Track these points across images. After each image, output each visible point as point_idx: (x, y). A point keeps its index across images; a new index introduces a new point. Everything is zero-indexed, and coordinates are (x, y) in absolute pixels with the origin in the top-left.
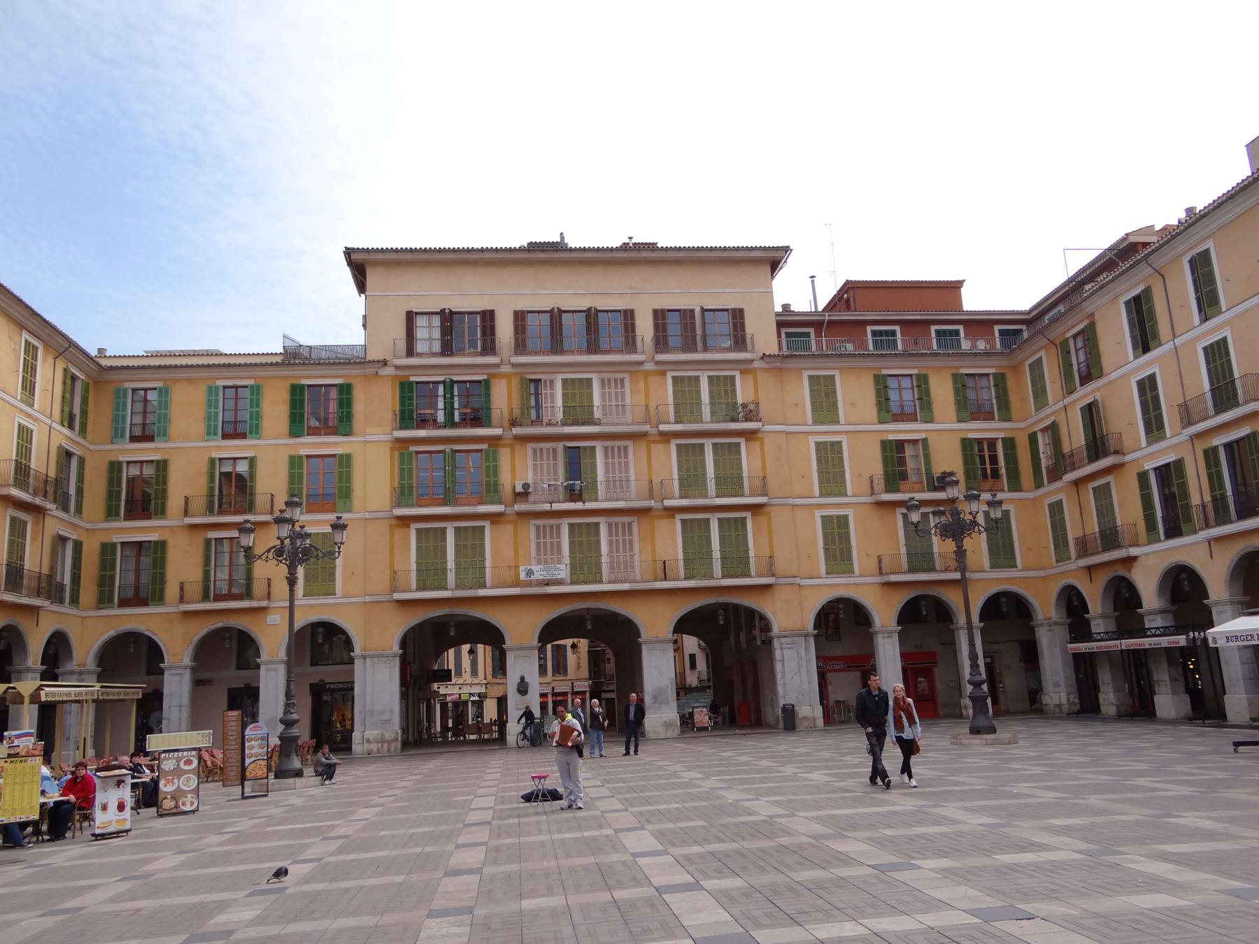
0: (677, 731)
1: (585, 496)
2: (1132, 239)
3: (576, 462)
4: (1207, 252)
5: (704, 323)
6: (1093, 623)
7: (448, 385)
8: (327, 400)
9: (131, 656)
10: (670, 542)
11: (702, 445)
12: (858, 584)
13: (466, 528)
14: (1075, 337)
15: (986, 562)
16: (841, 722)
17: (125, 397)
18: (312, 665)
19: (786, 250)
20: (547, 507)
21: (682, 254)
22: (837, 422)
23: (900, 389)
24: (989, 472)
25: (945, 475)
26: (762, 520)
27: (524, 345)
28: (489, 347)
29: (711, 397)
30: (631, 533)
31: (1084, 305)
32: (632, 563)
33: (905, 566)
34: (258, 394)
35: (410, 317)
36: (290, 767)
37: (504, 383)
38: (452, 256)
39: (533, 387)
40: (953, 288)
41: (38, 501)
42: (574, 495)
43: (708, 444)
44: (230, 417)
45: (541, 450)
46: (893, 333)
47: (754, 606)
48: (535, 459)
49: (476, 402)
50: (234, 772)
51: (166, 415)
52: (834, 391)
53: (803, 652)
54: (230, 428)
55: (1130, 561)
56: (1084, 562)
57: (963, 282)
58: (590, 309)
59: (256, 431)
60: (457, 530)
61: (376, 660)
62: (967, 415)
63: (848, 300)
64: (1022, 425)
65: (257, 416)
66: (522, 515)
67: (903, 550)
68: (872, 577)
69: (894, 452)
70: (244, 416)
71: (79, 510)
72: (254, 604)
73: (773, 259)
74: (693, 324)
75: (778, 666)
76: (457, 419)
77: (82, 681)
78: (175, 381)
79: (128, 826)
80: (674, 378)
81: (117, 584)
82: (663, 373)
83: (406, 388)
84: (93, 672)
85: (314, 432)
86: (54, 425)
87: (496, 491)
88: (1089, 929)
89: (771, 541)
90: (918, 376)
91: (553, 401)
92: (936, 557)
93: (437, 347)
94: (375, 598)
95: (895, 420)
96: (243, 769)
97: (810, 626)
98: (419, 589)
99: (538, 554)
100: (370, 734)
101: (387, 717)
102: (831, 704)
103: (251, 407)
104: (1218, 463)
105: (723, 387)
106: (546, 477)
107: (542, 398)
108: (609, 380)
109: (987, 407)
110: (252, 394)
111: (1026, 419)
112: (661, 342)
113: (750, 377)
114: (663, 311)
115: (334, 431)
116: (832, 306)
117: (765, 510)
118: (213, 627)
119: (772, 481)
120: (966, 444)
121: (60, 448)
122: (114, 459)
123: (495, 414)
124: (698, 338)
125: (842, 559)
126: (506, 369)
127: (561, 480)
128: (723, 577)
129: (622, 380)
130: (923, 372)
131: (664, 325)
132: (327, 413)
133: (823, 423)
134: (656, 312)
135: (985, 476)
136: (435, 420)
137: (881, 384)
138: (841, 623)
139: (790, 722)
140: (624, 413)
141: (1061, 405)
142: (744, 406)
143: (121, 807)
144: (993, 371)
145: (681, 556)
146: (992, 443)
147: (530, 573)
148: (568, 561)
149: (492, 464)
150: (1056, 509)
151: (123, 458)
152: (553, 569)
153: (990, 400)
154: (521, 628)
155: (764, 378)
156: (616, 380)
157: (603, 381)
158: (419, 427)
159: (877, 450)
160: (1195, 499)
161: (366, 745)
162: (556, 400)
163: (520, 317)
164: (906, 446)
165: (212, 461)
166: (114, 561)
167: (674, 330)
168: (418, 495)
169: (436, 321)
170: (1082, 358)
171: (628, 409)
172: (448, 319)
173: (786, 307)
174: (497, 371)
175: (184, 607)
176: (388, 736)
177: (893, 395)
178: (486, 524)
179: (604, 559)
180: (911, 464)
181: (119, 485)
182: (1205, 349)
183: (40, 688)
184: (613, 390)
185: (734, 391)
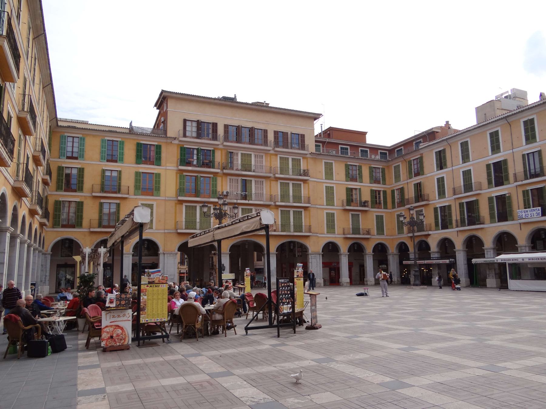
2: (434, 130)
3: (245, 185)
4: (467, 141)
6: (410, 255)
8: (150, 151)
11: (289, 183)
12: (337, 238)
14: (414, 160)
22: (333, 180)
28: (215, 137)
29: (292, 166)
33: (351, 232)
34: (123, 145)
35: (185, 121)
40: (363, 134)
42: (245, 197)
44: (110, 153)
46: (347, 149)
48: (230, 182)
52: (332, 168)
54: (110, 158)
59: (122, 160)
62: (349, 179)
67: (351, 227)
69: (350, 191)
73: (316, 117)
80: (280, 157)
82: (276, 155)
88: (358, 364)
89: (310, 219)
90: (382, 168)
91: (237, 161)
93: (195, 135)
101: (172, 277)
104: (463, 207)
105: (297, 162)
109: (355, 177)
111: (392, 185)
113: (305, 160)
122: (60, 165)
123: (216, 164)
126: (221, 147)
129: (262, 156)
131: (278, 137)
137: (347, 167)
141: (406, 182)
142: (304, 171)
146: (379, 191)
151: (64, 165)
155: (310, 161)
157: (255, 156)
160: (454, 218)
162: (238, 161)
163: (226, 127)
169: (195, 124)
170: (416, 167)
172: (199, 124)
182: (463, 172)
185: (300, 165)
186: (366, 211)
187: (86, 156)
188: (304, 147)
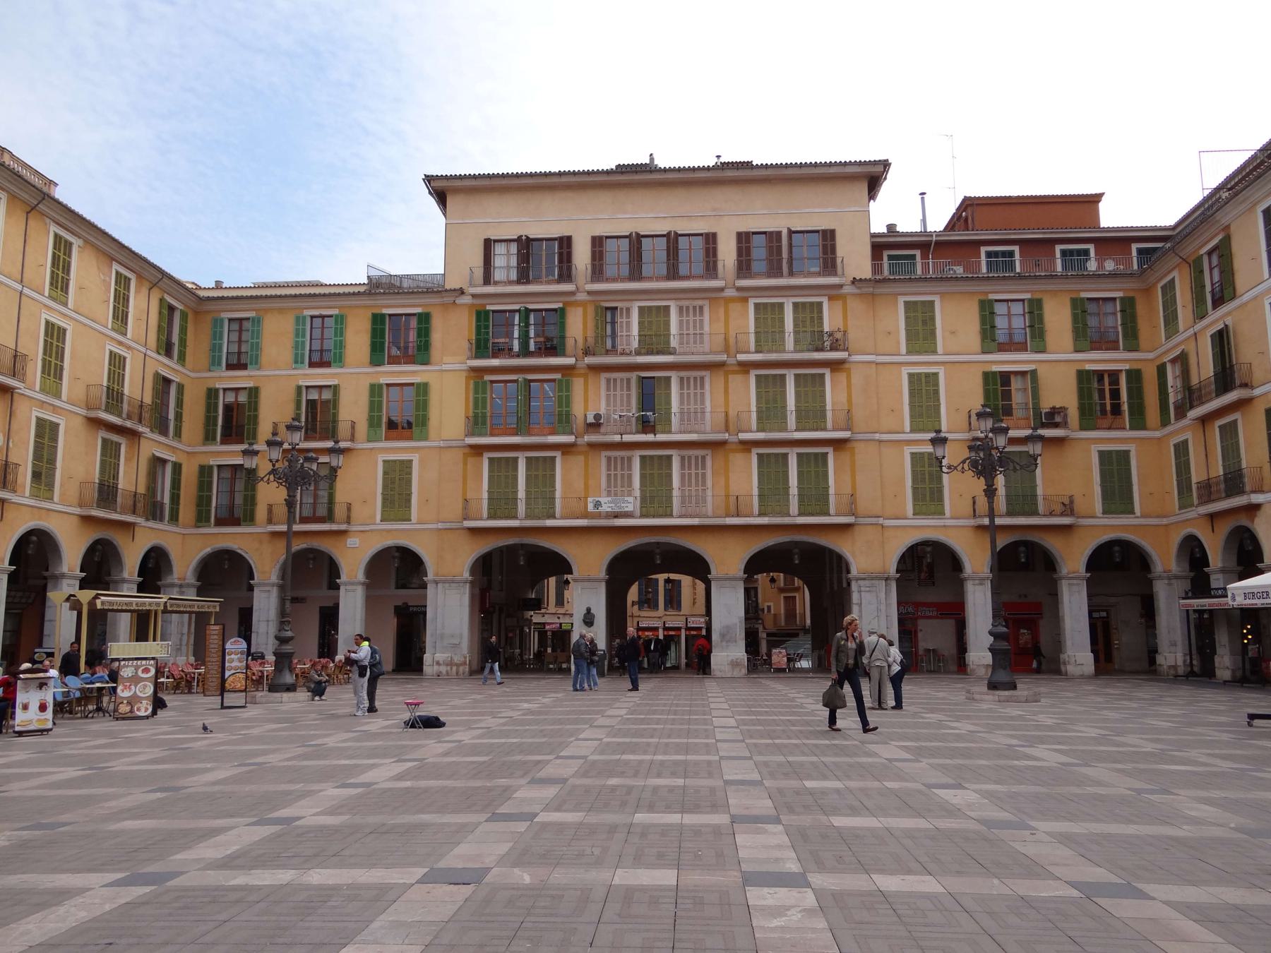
0: (744, 671)
1: (658, 427)
5: (790, 246)
6: (1212, 577)
7: (523, 314)
8: (408, 329)
9: (224, 572)
10: (745, 477)
11: (783, 376)
13: (537, 458)
14: (1210, 253)
16: (930, 672)
17: (222, 327)
18: (397, 588)
19: (886, 165)
20: (617, 438)
21: (769, 172)
22: (934, 352)
23: (1009, 315)
25: (1054, 412)
26: (845, 456)
27: (601, 271)
28: (566, 274)
29: (796, 325)
30: (704, 467)
31: (1218, 215)
35: (488, 244)
36: (282, 681)
37: (580, 311)
38: (473, 183)
39: (608, 315)
41: (128, 424)
43: (790, 376)
45: (615, 380)
46: (1011, 254)
47: (831, 547)
48: (608, 389)
49: (552, 331)
50: (214, 682)
51: (258, 344)
52: (933, 319)
53: (883, 595)
54: (316, 358)
55: (1254, 509)
56: (1205, 509)
57: (1101, 195)
58: (669, 233)
59: (339, 360)
65: (341, 345)
66: (593, 446)
68: (959, 520)
70: (329, 344)
71: (178, 434)
72: (334, 527)
73: (871, 177)
74: (779, 248)
76: (532, 347)
77: (182, 593)
78: (266, 310)
79: (50, 725)
80: (757, 306)
81: (214, 504)
82: (745, 300)
83: (482, 316)
84: (193, 586)
85: (394, 361)
86: (149, 352)
87: (568, 421)
90: (1030, 300)
92: (1040, 499)
93: (514, 275)
94: (448, 525)
95: (1000, 350)
96: (223, 680)
97: (892, 569)
98: (490, 517)
99: (609, 486)
100: (440, 656)
102: (921, 652)
103: (336, 335)
105: (809, 314)
106: (618, 408)
107: (618, 326)
108: (688, 308)
110: (336, 323)
112: (744, 267)
114: (601, 238)
115: (411, 360)
116: (951, 226)
117: (849, 445)
119: (858, 414)
121: (157, 375)
122: (211, 386)
123: (570, 343)
125: (932, 499)
126: (581, 297)
127: (633, 411)
128: (800, 515)
129: (701, 308)
130: (1037, 296)
132: (407, 342)
133: (919, 353)
134: (739, 235)
135: (1103, 411)
136: (511, 350)
137: (987, 311)
138: (927, 568)
139: (676, 668)
140: (702, 342)
141: (1191, 331)
142: (831, 334)
143: (43, 708)
145: (755, 491)
146: (1114, 375)
147: (598, 504)
148: (637, 493)
149: (991, 387)
150: (1182, 449)
152: (620, 501)
153: (1116, 327)
154: (727, 560)
156: (694, 308)
157: (681, 308)
158: (495, 356)
159: (979, 381)
161: (436, 667)
162: (632, 328)
164: (1013, 379)
165: (299, 388)
166: (211, 483)
167: (759, 251)
168: (492, 425)
169: (514, 248)
170: (1216, 278)
171: (706, 338)
172: (526, 246)
173: (891, 228)
174: (573, 299)
175: (271, 528)
176: (457, 659)
177: (1001, 323)
178: (558, 454)
179: (676, 493)
180: (1017, 398)
181: (216, 410)
183: (97, 597)
184: (691, 318)
185: (821, 318)
187: (264, 359)
188: (834, 265)
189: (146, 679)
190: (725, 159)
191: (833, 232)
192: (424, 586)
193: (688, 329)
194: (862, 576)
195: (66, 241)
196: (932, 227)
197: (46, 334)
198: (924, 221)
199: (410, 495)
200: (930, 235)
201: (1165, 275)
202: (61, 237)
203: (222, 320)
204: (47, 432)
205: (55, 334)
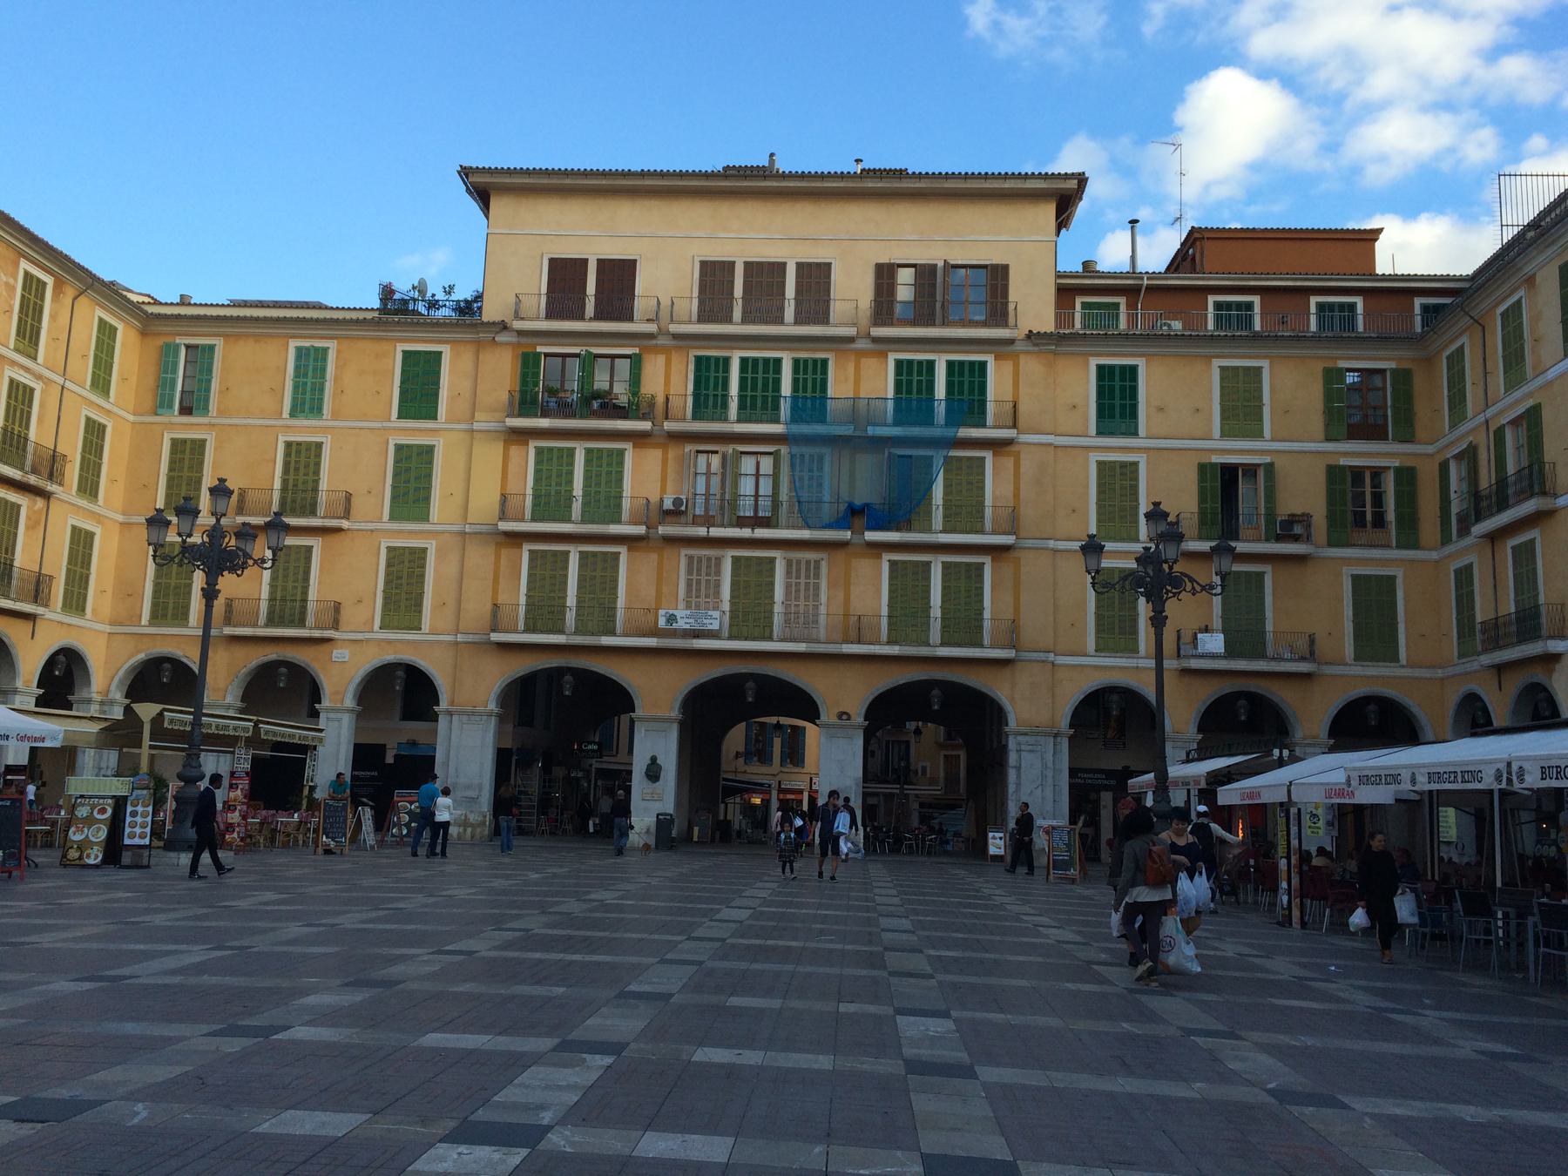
12: (427, 644)
15: (1349, 650)
20: (701, 531)
22: (1135, 434)
24: (1369, 517)
25: (1292, 520)
29: (795, 388)
30: (817, 576)
32: (816, 615)
37: (661, 360)
41: (33, 480)
46: (1249, 306)
53: (1049, 757)
60: (946, 566)
61: (465, 718)
63: (1193, 259)
64: (1430, 449)
74: (934, 285)
75: (1012, 775)
83: (529, 363)
97: (1064, 723)
98: (527, 630)
101: (473, 794)
118: (266, 659)
119: (1028, 513)
120: (1335, 474)
124: (938, 305)
133: (1111, 434)
141: (1481, 419)
144: (1393, 365)
145: (885, 611)
146: (1377, 473)
148: (726, 606)
159: (1193, 476)
176: (472, 818)
179: (778, 608)
183: (161, 714)
186: (1300, 559)
188: (1005, 314)
189: (100, 821)
190: (868, 164)
191: (1005, 268)
192: (434, 718)
193: (805, 390)
194: (1022, 729)
195: (39, 280)
196: (1142, 266)
197: (86, 431)
198: (1133, 258)
199: (421, 595)
200: (1140, 276)
201: (1452, 341)
202: (32, 276)
203: (177, 347)
204: (82, 542)
205: (95, 431)
